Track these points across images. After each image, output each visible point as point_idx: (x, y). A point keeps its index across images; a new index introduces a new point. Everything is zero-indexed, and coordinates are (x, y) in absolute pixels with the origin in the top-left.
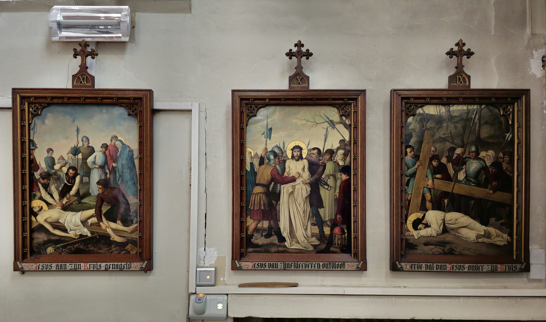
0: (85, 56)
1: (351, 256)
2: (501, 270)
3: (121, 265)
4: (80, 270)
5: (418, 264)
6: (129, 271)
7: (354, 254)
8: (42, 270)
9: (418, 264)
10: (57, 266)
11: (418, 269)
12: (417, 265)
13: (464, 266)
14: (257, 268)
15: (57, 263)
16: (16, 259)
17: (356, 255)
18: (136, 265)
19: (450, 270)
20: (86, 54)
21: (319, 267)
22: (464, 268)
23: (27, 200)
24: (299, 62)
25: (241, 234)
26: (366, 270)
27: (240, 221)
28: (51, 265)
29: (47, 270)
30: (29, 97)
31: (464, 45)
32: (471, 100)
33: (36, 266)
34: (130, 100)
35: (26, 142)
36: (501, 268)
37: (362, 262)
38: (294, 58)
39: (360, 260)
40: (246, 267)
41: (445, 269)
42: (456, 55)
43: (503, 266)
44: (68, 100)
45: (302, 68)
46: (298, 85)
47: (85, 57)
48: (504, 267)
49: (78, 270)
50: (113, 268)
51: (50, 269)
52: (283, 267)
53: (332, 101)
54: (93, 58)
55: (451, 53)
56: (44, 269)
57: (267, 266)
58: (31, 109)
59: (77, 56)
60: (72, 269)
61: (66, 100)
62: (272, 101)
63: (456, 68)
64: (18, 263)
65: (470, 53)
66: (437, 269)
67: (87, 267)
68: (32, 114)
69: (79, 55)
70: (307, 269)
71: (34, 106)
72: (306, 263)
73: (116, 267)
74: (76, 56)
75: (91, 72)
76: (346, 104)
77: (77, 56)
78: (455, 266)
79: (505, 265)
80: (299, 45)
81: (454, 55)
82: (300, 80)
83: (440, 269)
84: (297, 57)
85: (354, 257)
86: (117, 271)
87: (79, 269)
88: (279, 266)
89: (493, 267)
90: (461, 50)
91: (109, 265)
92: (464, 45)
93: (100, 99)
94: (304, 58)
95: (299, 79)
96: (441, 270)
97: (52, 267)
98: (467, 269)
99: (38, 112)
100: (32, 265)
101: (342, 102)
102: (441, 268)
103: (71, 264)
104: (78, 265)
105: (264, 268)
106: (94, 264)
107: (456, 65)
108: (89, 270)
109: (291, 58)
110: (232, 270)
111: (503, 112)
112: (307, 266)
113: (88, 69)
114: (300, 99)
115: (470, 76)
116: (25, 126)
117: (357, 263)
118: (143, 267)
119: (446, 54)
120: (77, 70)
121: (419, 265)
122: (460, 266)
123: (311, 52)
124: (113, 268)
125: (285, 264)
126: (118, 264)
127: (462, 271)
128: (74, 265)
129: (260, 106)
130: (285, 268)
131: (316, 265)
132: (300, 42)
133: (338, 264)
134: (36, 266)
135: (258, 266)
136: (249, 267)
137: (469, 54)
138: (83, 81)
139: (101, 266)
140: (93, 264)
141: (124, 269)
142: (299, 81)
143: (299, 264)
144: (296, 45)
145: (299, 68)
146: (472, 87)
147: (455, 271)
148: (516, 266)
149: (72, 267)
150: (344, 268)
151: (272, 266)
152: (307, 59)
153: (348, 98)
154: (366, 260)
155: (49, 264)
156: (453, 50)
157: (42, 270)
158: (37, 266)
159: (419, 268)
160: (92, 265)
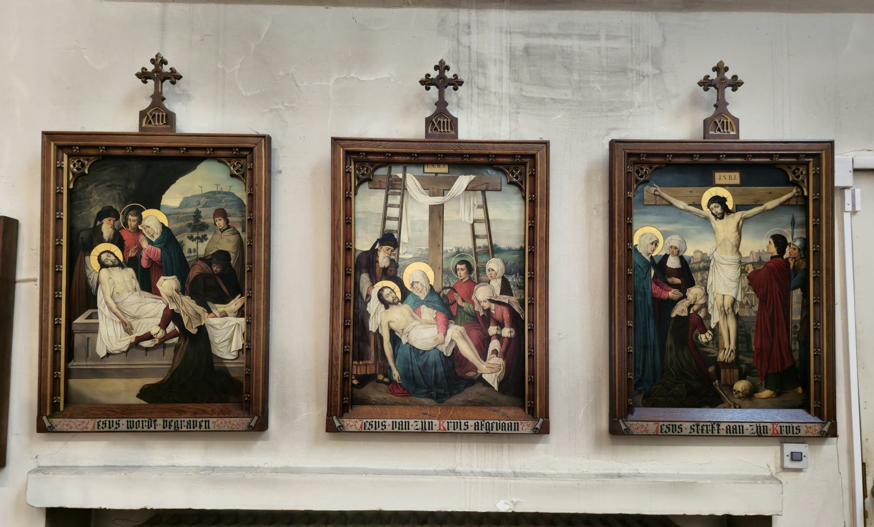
0: (161, 80)
1: (525, 411)
2: (773, 433)
3: (138, 422)
4: (766, 435)
5: (150, 421)
6: (679, 435)
7: (529, 408)
8: (382, 430)
9: (498, 422)
10: (727, 429)
11: (674, 433)
12: (148, 421)
13: (680, 426)
14: (666, 432)
15: (401, 420)
16: (330, 414)
17: (819, 413)
18: (241, 422)
19: (93, 430)
20: (162, 77)
21: (431, 428)
22: (681, 429)
23: (62, 316)
24: (441, 95)
25: (343, 373)
26: (549, 434)
27: (344, 351)
28: (119, 421)
29: (112, 429)
30: (70, 147)
31: (727, 69)
32: (482, 159)
33: (658, 427)
34: (438, 157)
35: (64, 219)
36: (773, 429)
37: (541, 420)
38: (433, 88)
39: (538, 416)
40: (643, 429)
41: (741, 432)
42: (715, 86)
43: (444, 422)
44: (132, 150)
45: (447, 104)
46: (433, 131)
47: (160, 82)
48: (445, 425)
49: (763, 435)
50: (129, 427)
51: (116, 428)
52: (421, 427)
53: (726, 158)
54: (173, 83)
55: (706, 84)
56: (106, 427)
57: (389, 425)
58: (72, 166)
59: (147, 80)
60: (417, 429)
61: (155, 152)
62: (501, 159)
63: (716, 106)
64: (44, 418)
65: (456, 82)
66: (165, 426)
67: (444, 427)
68: (73, 174)
69: (150, 78)
70: (167, 429)
71: (78, 161)
72: (498, 422)
73: (508, 428)
74: (146, 79)
75: (453, 111)
76: (517, 164)
77: (147, 80)
78: (665, 426)
79: (447, 421)
80: (720, 69)
81: (711, 86)
82: (437, 124)
83: (502, 430)
84: (438, 87)
85: (529, 413)
86: (405, 432)
87: (764, 433)
88: (412, 425)
89: (131, 424)
90: (442, 77)
91: (169, 422)
92: (447, 68)
93: (157, 149)
94: (167, 84)
95: (718, 123)
96: (189, 429)
97: (683, 430)
98: (473, 428)
99: (84, 170)
100: (356, 422)
101: (794, 160)
102: (504, 428)
103: (416, 422)
104: (429, 422)
105: (678, 432)
106: (791, 426)
107: (715, 102)
108: (448, 431)
109: (428, 89)
110: (326, 432)
111: (793, 177)
112: (168, 425)
113: (165, 101)
114: (647, 154)
115: (738, 119)
116: (62, 193)
117: (249, 420)
118: (824, 431)
119: (699, 83)
120: (146, 103)
121: (500, 423)
122: (674, 427)
123: (741, 80)
124: (206, 428)
125: (425, 422)
126: (190, 421)
127: (678, 434)
128: (422, 422)
129: (378, 164)
130: (489, 430)
131: (203, 424)
132: (721, 63)
133: (488, 422)
134: (658, 427)
135: (668, 429)
136: (648, 429)
137: (456, 83)
138: (153, 120)
139: (119, 424)
140: (143, 421)
141: (492, 430)
142: (436, 125)
143: (365, 423)
144: (714, 69)
145: (441, 104)
146: (742, 138)
147: (102, 430)
148: (799, 426)
149: (752, 429)
150: (155, 428)
151: (502, 428)
152: (456, 89)
153: (700, 154)
154: (548, 418)
155: (115, 420)
156: (709, 79)
157: (382, 430)
158: (363, 424)
159: (457, 428)
160: (452, 424)
